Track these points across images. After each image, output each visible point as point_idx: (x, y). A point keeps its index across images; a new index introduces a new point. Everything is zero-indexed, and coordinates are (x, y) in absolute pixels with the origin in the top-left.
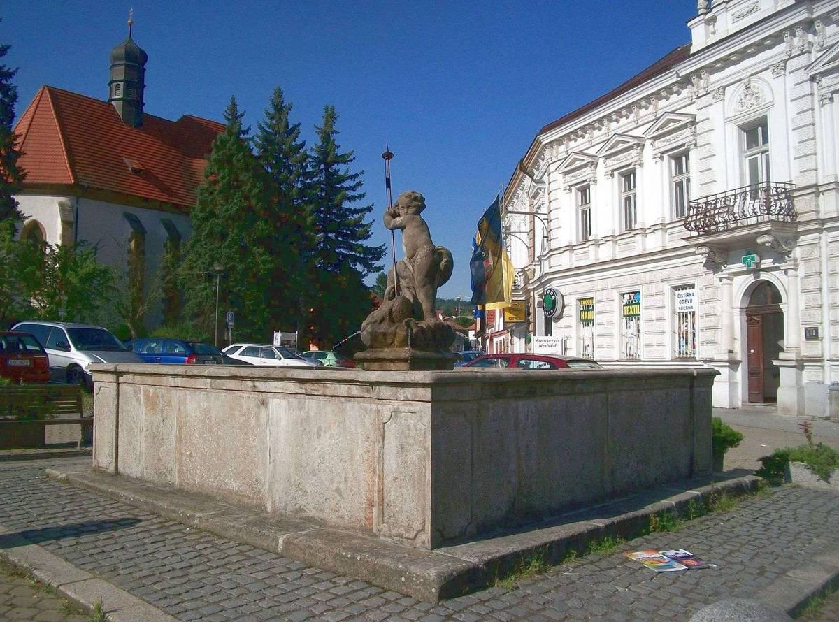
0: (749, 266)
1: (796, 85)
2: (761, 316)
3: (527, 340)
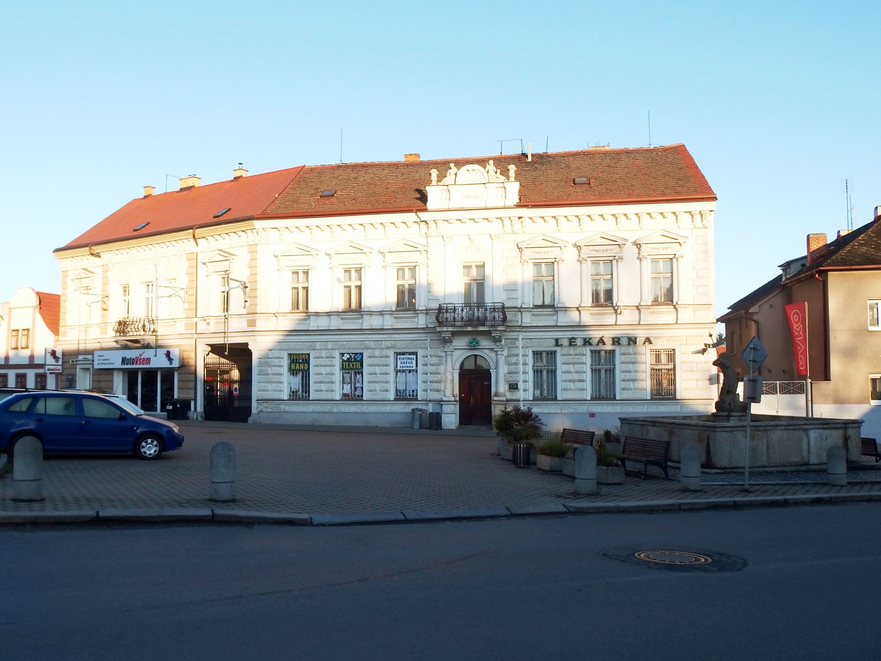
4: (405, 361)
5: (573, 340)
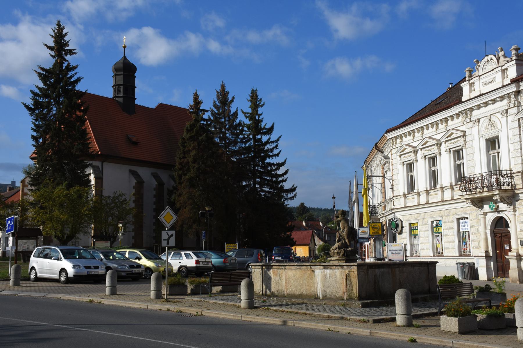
0: (492, 209)
1: (512, 122)
3: (383, 245)
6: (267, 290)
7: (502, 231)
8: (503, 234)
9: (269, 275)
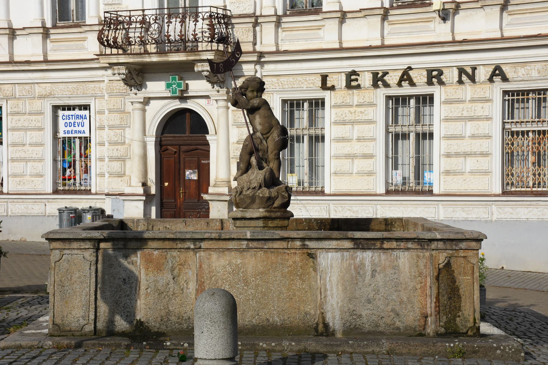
2: (178, 147)
4: (72, 121)
5: (353, 77)
6: (118, 318)
7: (184, 140)
8: (184, 148)
9: (126, 269)
